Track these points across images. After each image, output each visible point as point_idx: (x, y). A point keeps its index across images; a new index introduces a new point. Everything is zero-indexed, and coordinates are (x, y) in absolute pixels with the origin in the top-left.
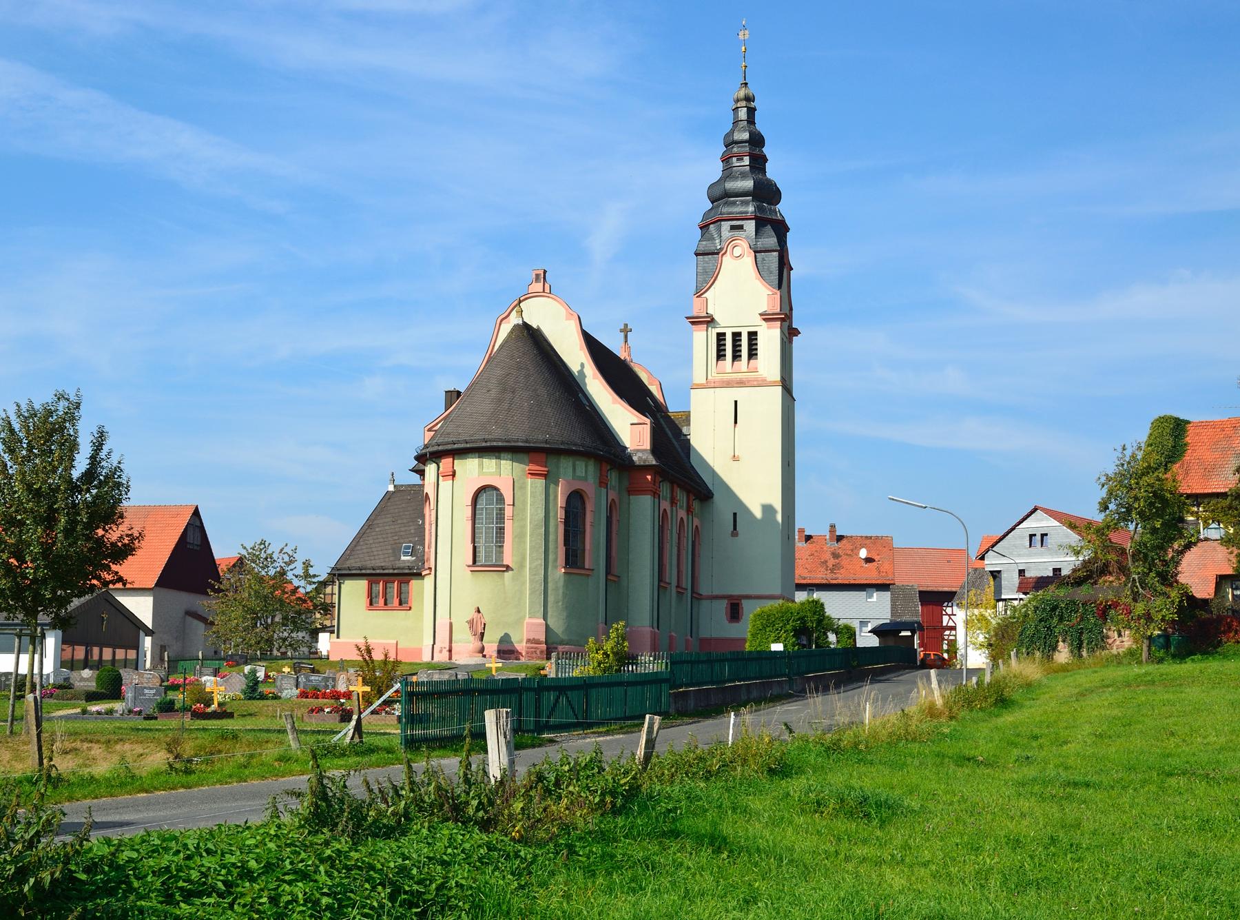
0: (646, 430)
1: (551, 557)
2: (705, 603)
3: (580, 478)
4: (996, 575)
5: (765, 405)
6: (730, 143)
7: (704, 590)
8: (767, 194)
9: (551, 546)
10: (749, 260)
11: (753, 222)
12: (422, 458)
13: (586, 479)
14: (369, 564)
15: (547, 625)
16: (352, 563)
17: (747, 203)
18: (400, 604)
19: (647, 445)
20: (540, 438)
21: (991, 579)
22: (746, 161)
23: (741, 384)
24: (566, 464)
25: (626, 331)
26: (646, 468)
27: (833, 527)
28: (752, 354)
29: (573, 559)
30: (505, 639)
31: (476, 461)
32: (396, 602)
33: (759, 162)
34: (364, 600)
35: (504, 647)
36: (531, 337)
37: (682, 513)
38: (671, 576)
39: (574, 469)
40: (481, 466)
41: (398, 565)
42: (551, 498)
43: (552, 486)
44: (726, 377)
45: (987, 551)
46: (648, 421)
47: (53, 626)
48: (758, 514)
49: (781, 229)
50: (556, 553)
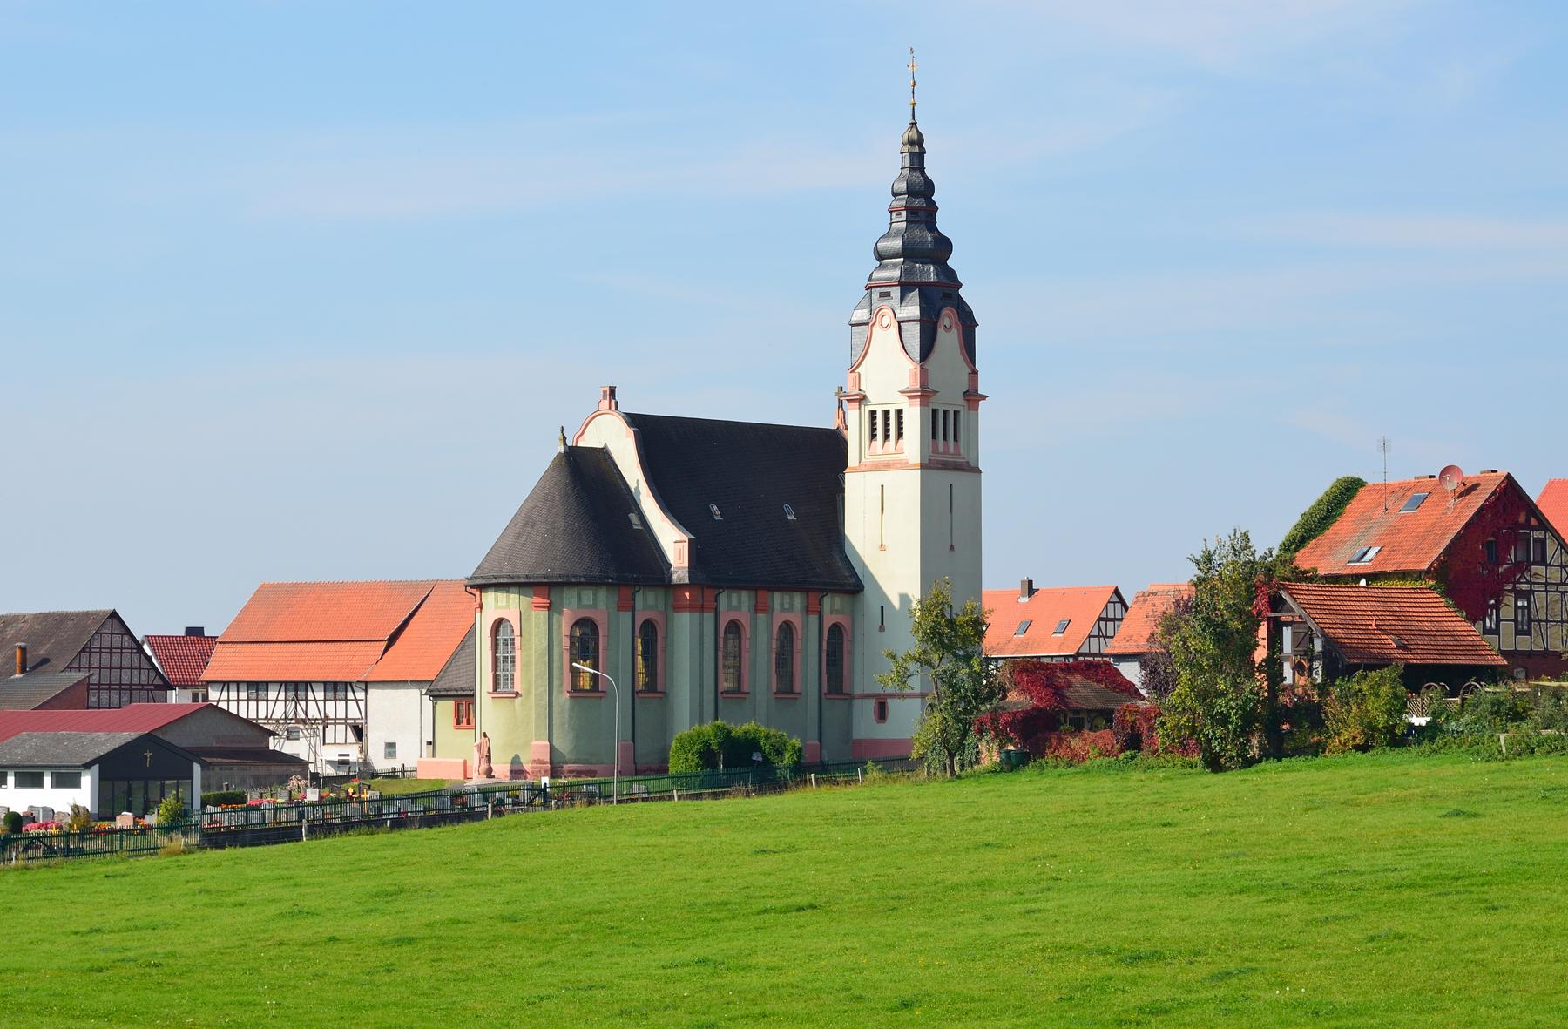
1: (556, 683)
3: (587, 607)
7: (857, 690)
9: (556, 672)
13: (594, 606)
15: (552, 747)
20: (540, 573)
23: (887, 466)
24: (570, 595)
28: (900, 435)
30: (516, 760)
34: (452, 720)
35: (516, 768)
39: (579, 599)
42: (555, 627)
43: (556, 616)
44: (876, 459)
48: (897, 604)
50: (561, 680)
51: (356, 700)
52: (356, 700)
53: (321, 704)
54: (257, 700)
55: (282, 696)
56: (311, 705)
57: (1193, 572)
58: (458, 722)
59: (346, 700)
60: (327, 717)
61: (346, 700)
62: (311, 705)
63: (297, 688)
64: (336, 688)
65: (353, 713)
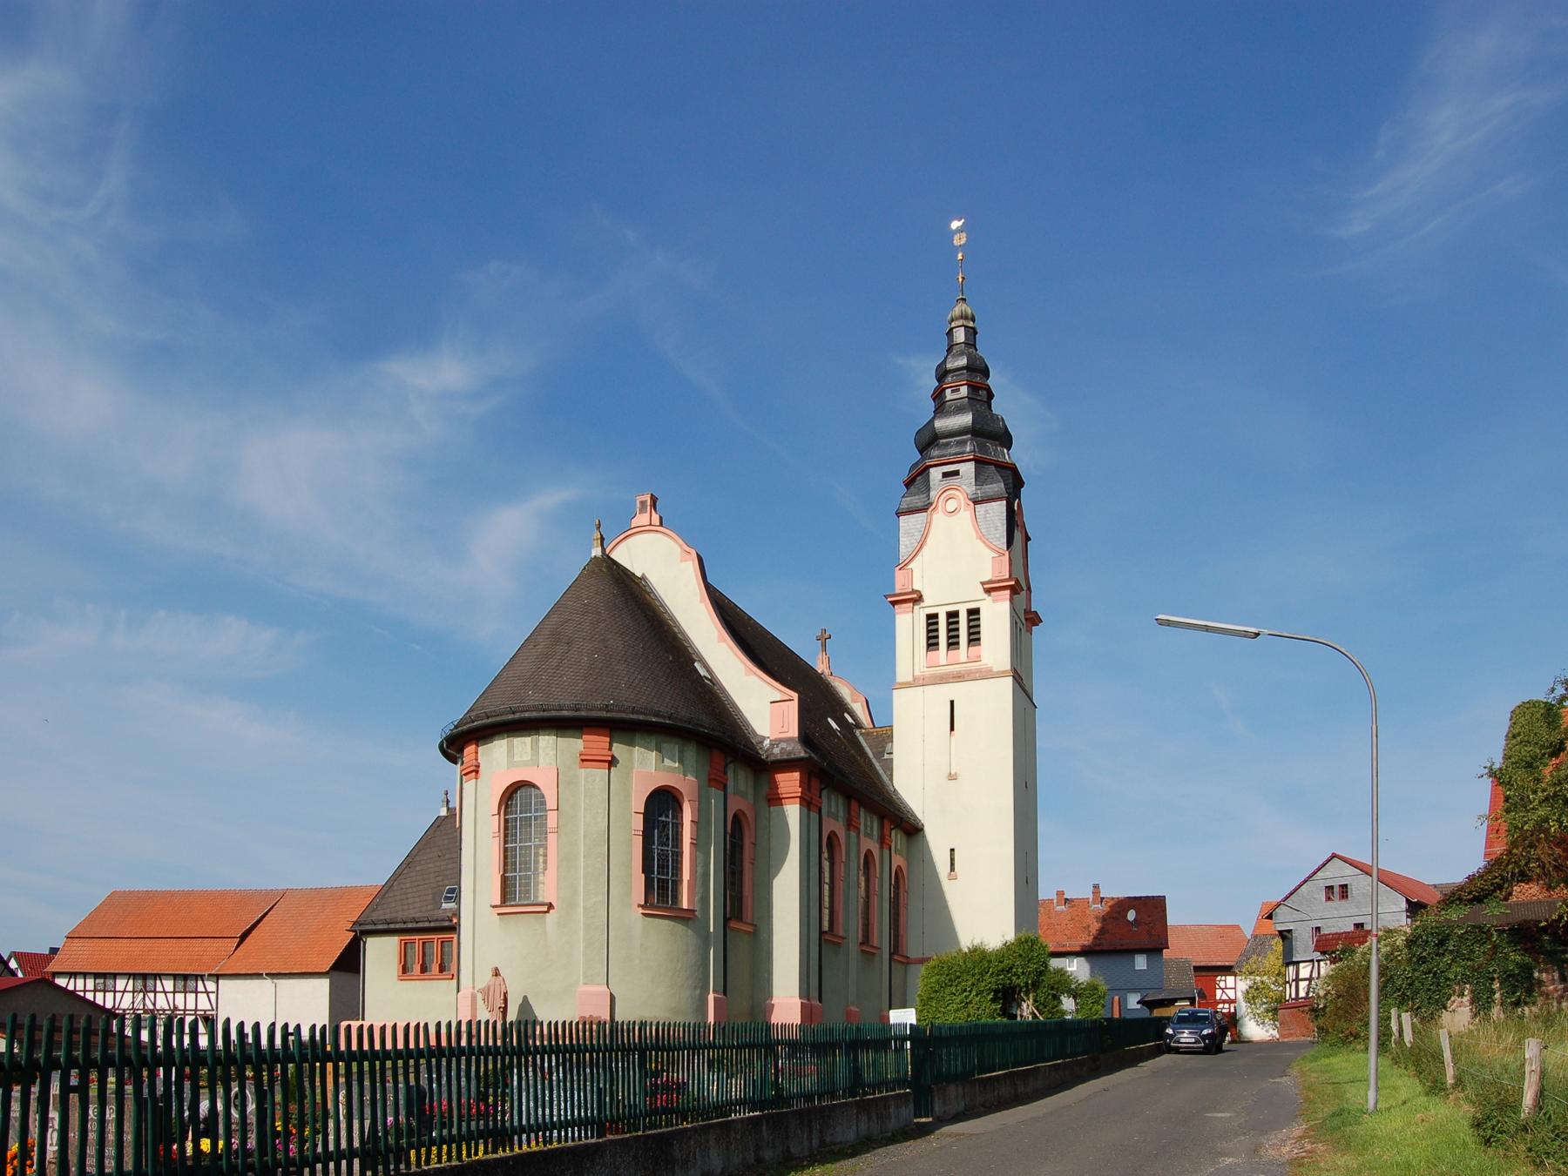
0: (793, 708)
2: (912, 967)
4: (1285, 936)
5: (990, 705)
6: (942, 373)
7: (913, 951)
8: (990, 435)
10: (966, 515)
11: (971, 465)
12: (455, 745)
14: (400, 915)
16: (378, 915)
17: (964, 443)
18: (442, 969)
19: (793, 731)
21: (1278, 940)
22: (964, 391)
23: (959, 677)
25: (824, 639)
26: (787, 765)
27: (1096, 887)
28: (974, 638)
29: (660, 888)
31: (528, 740)
32: (417, 968)
33: (981, 395)
34: (394, 967)
36: (629, 595)
37: (871, 845)
38: (851, 928)
40: (535, 748)
41: (438, 914)
45: (1278, 905)
46: (795, 695)
47: (1466, 979)
49: (1014, 482)
51: (207, 993)
52: (207, 993)
53: (170, 996)
54: (105, 991)
55: (130, 988)
56: (160, 997)
57: (1488, 783)
58: (405, 969)
59: (196, 992)
60: (176, 1008)
61: (196, 992)
62: (160, 997)
63: (145, 979)
64: (185, 980)
65: (204, 1004)
